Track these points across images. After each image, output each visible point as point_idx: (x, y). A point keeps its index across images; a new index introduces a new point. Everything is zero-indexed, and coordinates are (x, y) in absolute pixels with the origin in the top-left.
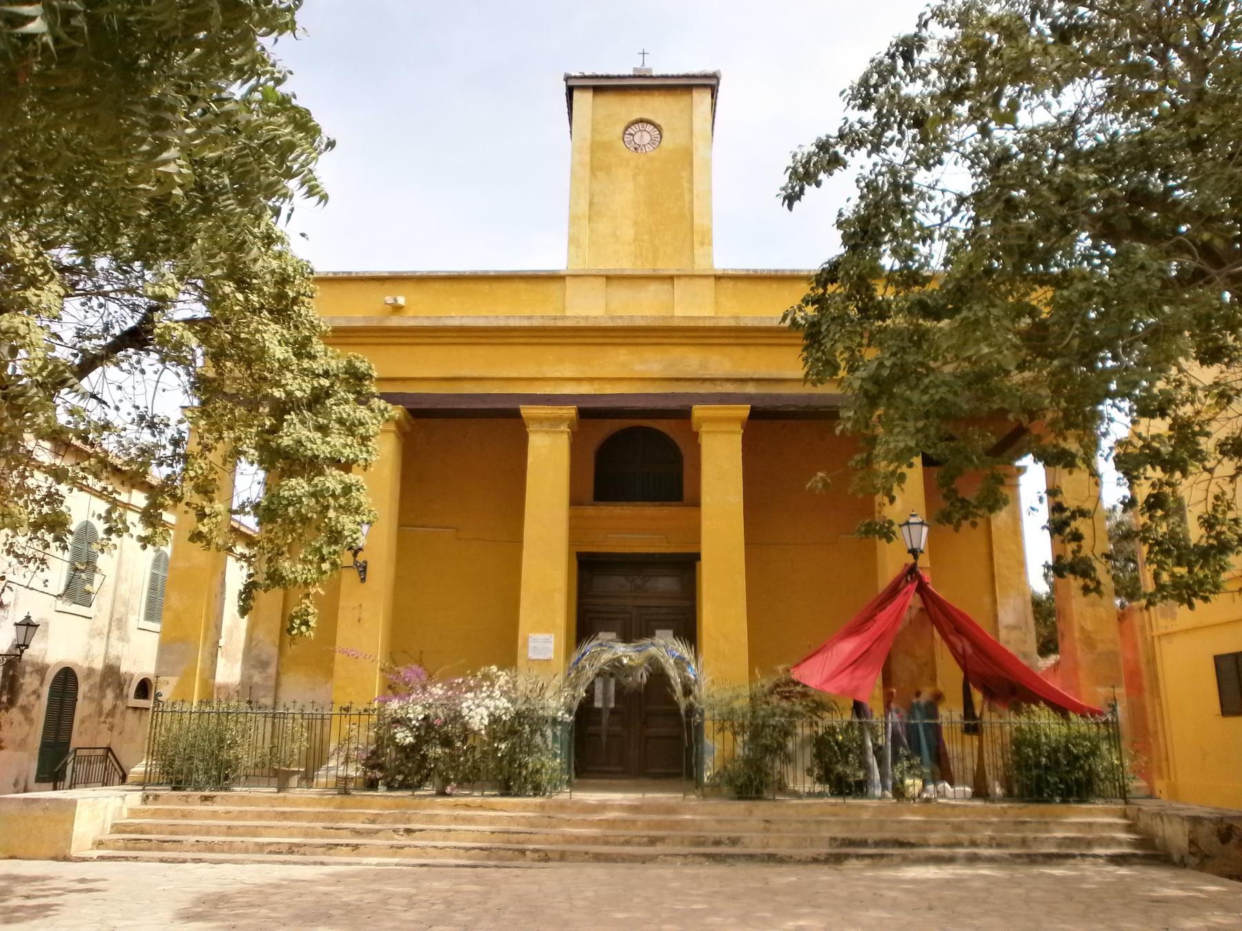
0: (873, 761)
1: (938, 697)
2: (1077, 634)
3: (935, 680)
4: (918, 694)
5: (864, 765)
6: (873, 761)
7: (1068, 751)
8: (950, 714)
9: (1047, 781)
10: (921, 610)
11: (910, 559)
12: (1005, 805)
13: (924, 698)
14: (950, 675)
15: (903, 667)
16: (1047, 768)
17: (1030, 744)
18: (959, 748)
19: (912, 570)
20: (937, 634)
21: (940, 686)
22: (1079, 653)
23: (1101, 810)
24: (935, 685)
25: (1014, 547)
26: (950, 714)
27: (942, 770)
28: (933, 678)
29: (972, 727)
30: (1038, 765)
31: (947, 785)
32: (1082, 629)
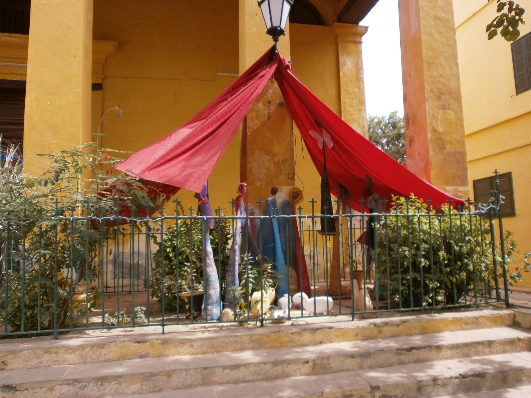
0: (213, 271)
1: (296, 195)
2: (429, 135)
3: (293, 178)
4: (274, 192)
5: (201, 275)
6: (213, 271)
7: (449, 248)
8: (308, 221)
9: (426, 286)
10: (281, 105)
11: (269, 42)
12: (378, 321)
13: (281, 197)
14: (308, 178)
15: (260, 164)
16: (427, 270)
17: (405, 242)
18: (317, 252)
19: (271, 56)
20: (296, 132)
21: (298, 184)
22: (431, 153)
23: (487, 318)
24: (294, 184)
25: (356, 90)
26: (308, 221)
27: (298, 279)
28: (292, 177)
29: (330, 226)
30: (415, 266)
31: (304, 295)
32: (434, 131)
